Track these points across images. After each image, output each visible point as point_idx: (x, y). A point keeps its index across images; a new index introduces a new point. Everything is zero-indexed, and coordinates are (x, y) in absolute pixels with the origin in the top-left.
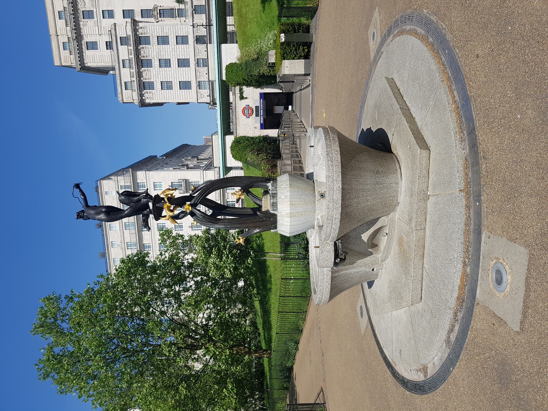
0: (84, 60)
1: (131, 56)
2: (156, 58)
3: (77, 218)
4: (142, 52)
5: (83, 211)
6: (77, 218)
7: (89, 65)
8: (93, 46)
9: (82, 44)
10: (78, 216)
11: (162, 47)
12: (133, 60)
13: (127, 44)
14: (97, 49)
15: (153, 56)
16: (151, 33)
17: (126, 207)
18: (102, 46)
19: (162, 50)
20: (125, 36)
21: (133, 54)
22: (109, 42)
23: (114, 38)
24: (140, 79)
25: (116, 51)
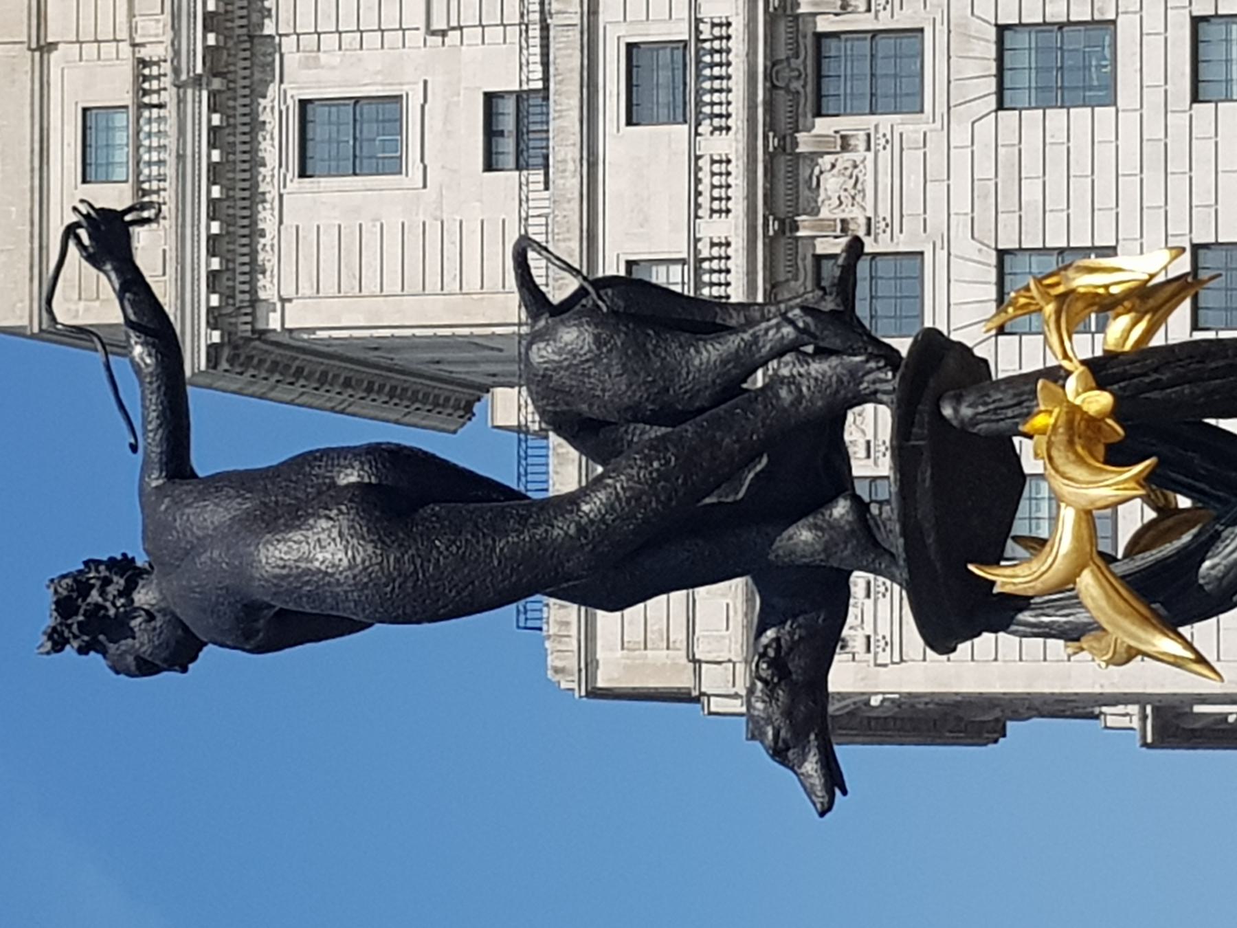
0: (255, 268)
1: (712, 228)
2: (962, 243)
3: (58, 641)
4: (831, 185)
5: (123, 565)
6: (58, 641)
7: (300, 316)
8: (358, 136)
9: (255, 126)
10: (64, 607)
11: (1031, 125)
12: (738, 45)
13: (688, 110)
14: (395, 166)
15: (937, 219)
16: (937, 219)
17: (565, 469)
18: (449, 133)
19: (1032, 165)
20: (681, 32)
21: (738, 206)
22: (520, 96)
23: (567, 58)
24: (789, 226)
25: (568, 180)
